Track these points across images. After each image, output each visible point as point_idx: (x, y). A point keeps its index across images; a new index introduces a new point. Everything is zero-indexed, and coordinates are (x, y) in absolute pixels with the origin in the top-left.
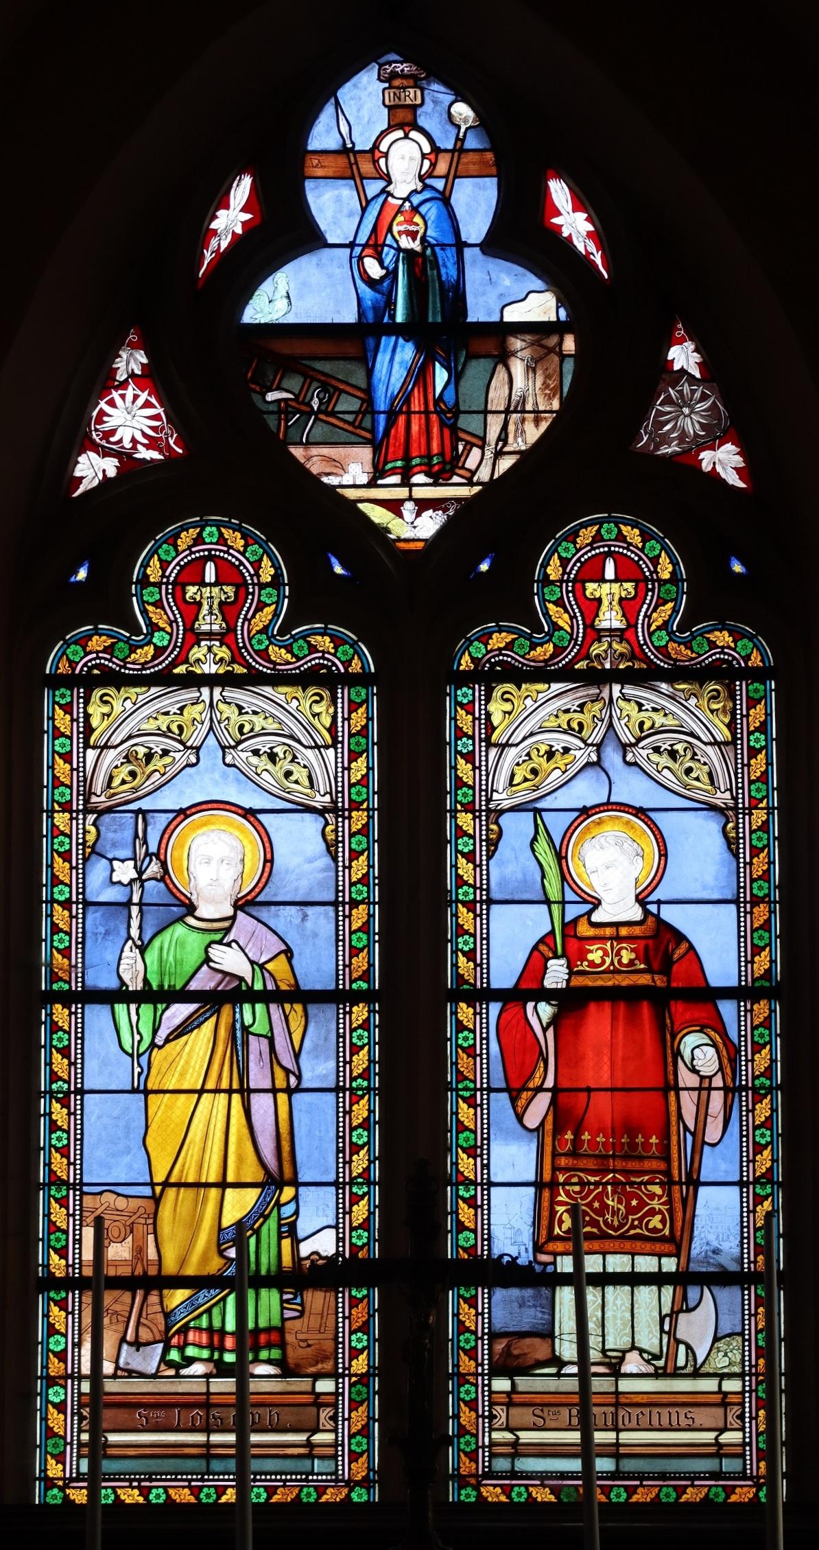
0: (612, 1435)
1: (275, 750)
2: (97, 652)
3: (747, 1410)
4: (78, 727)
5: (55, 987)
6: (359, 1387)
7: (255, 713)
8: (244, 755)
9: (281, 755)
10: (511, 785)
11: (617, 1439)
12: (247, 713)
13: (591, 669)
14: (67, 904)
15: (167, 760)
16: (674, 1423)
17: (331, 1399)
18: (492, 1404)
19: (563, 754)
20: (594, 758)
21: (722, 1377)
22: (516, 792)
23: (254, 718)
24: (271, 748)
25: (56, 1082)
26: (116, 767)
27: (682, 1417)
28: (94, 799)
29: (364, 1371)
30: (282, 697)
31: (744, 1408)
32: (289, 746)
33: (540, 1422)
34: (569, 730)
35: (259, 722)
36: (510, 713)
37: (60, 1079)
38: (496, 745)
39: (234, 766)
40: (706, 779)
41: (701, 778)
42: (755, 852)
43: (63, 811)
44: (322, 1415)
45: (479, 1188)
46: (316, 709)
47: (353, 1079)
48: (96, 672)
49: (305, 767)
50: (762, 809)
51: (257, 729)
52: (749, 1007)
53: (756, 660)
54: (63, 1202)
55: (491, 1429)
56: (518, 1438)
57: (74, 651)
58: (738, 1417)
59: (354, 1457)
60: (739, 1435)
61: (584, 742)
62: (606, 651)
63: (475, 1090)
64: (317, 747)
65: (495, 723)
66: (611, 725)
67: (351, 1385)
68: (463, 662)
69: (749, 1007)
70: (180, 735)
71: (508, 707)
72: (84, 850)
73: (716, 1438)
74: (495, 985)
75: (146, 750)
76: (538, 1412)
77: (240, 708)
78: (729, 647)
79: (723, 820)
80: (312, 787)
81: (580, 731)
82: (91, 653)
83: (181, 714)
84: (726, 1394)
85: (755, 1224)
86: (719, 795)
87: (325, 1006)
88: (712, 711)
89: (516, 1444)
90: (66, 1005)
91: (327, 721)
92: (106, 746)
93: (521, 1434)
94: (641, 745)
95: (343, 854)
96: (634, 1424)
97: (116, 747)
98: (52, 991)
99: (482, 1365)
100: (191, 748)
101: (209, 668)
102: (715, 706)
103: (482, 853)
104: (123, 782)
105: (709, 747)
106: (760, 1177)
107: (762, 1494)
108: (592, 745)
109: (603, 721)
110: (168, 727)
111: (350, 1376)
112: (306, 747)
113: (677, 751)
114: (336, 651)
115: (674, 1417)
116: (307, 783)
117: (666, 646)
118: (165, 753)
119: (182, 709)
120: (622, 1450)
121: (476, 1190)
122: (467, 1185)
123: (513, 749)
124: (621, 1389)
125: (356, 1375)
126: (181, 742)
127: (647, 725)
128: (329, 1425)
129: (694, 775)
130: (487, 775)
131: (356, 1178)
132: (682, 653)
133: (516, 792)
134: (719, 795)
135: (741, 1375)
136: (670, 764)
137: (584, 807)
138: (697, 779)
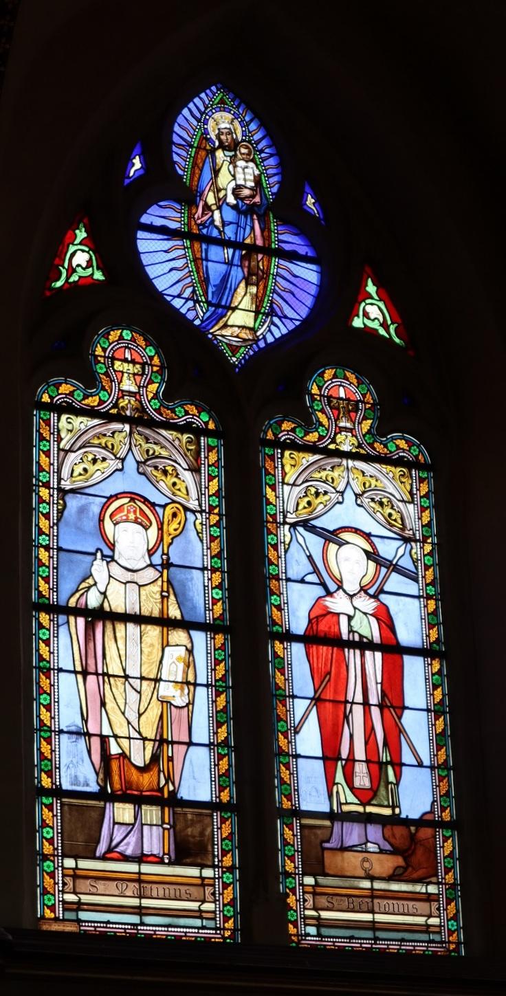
2: (288, 431)
3: (217, 889)
4: (54, 438)
7: (371, 476)
8: (149, 469)
9: (386, 504)
10: (72, 476)
11: (374, 919)
12: (151, 443)
14: (47, 548)
15: (327, 497)
16: (396, 910)
17: (211, 882)
18: (64, 876)
19: (102, 461)
20: (120, 466)
22: (74, 482)
23: (154, 446)
24: (164, 467)
26: (76, 464)
28: (63, 482)
29: (230, 864)
30: (385, 470)
31: (215, 888)
32: (174, 467)
33: (94, 890)
34: (105, 448)
37: (45, 660)
38: (63, 450)
39: (362, 506)
40: (184, 491)
41: (182, 489)
44: (207, 892)
45: (53, 734)
47: (216, 681)
48: (288, 441)
49: (398, 512)
50: (429, 543)
55: (305, 908)
56: (80, 899)
58: (66, 884)
61: (115, 456)
62: (127, 405)
66: (348, 482)
67: (446, 890)
68: (268, 434)
69: (212, 636)
71: (293, 463)
72: (284, 546)
73: (426, 921)
75: (93, 456)
76: (329, 899)
77: (363, 473)
80: (188, 494)
81: (333, 482)
87: (155, 627)
88: (402, 482)
90: (282, 642)
92: (70, 450)
93: (82, 897)
94: (366, 495)
96: (382, 910)
97: (75, 452)
99: (57, 849)
100: (119, 458)
101: (345, 448)
102: (190, 448)
104: (305, 508)
105: (187, 472)
108: (119, 458)
109: (125, 445)
110: (106, 444)
111: (222, 867)
115: (167, 891)
116: (185, 492)
118: (326, 493)
120: (144, 911)
124: (142, 871)
125: (448, 884)
126: (113, 454)
127: (151, 452)
128: (211, 898)
130: (283, 503)
133: (74, 482)
134: (407, 532)
136: (380, 510)
137: (154, 503)
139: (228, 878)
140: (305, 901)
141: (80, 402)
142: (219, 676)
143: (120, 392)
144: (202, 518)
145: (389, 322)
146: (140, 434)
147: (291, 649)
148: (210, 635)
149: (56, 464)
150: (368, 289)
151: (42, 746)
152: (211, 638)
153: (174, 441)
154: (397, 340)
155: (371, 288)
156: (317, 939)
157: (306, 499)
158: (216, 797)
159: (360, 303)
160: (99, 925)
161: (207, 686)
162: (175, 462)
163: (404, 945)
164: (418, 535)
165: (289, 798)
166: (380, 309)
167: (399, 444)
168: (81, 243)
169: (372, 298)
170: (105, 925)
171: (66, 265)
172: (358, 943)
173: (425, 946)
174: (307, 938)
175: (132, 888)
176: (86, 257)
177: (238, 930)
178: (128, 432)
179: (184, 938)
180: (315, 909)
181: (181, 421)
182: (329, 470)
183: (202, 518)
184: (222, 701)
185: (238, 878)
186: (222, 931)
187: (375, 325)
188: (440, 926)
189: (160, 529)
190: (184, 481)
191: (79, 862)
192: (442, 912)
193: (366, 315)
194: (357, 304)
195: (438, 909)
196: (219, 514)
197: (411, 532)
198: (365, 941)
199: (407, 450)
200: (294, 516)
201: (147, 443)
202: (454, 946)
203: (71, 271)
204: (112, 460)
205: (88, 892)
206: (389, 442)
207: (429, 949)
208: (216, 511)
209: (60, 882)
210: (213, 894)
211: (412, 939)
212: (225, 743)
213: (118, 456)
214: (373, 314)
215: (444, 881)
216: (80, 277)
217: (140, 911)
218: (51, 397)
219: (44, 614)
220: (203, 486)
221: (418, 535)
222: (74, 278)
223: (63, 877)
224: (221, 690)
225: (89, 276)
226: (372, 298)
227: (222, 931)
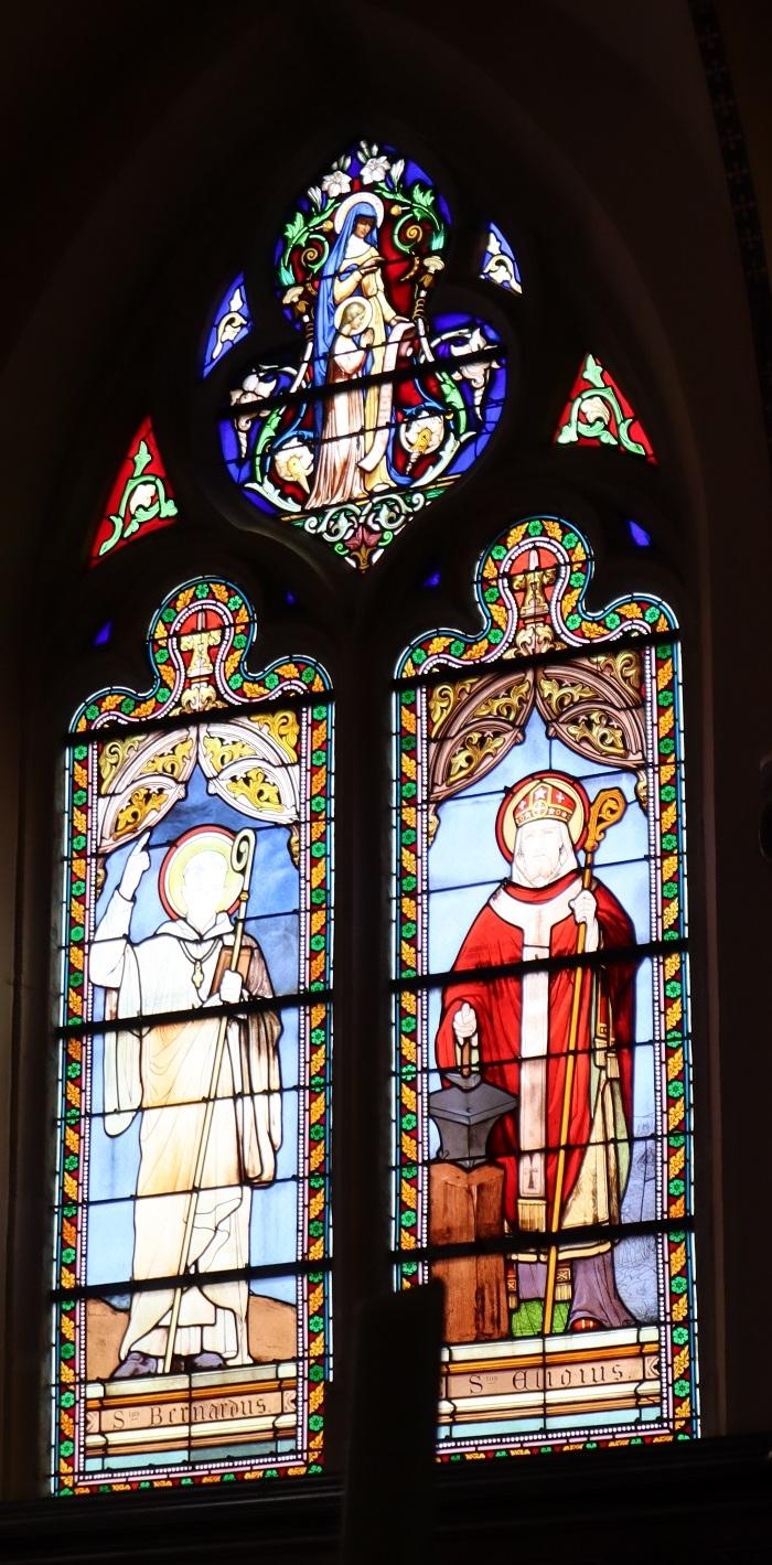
0: (540, 1396)
1: (249, 775)
2: (438, 654)
5: (404, 975)
6: (316, 1367)
7: (234, 743)
9: (597, 721)
10: (116, 831)
11: (190, 1433)
12: (567, 686)
13: (182, 714)
16: (598, 1378)
18: (87, 1410)
19: (158, 795)
21: (277, 1362)
23: (233, 748)
25: (406, 1066)
27: (254, 1405)
33: (119, 1425)
34: (156, 774)
35: (237, 750)
36: (116, 764)
42: (664, 805)
43: (80, 858)
46: (283, 730)
48: (435, 670)
51: (236, 757)
52: (661, 960)
53: (318, 687)
54: (413, 1182)
55: (87, 1434)
56: (455, 1407)
57: (92, 712)
59: (678, 1401)
60: (656, 1385)
63: (80, 1116)
64: (284, 765)
65: (104, 776)
66: (197, 762)
67: (310, 1367)
70: (172, 773)
73: (635, 1391)
74: (433, 971)
75: (480, 735)
77: (222, 740)
78: (296, 678)
79: (635, 781)
82: (432, 655)
83: (174, 754)
84: (282, 1380)
85: (668, 1176)
86: (631, 757)
89: (106, 1446)
90: (414, 992)
91: (294, 741)
92: (113, 794)
95: (304, 859)
98: (401, 979)
103: (91, 893)
106: (673, 1130)
107: (67, 1490)
111: (671, 1323)
112: (275, 766)
113: (593, 721)
114: (644, 615)
117: (580, 627)
119: (173, 749)
121: (77, 1209)
122: (411, 1166)
123: (118, 797)
125: (314, 1358)
129: (609, 741)
131: (314, 1172)
132: (253, 690)
135: (295, 1360)
138: (612, 745)
139: (681, 1336)
140: (295, 1401)
141: (459, 658)
142: (672, 1023)
143: (521, 622)
144: (648, 778)
145: (619, 418)
146: (548, 679)
147: (92, 1046)
148: (304, 1010)
149: (425, 765)
150: (586, 375)
151: (403, 1191)
152: (305, 1015)
153: (260, 729)
154: (631, 447)
155: (593, 371)
156: (186, 1468)
157: (133, 809)
158: (663, 1212)
159: (573, 401)
160: (619, 1429)
161: (297, 1088)
162: (605, 702)
163: (595, 1435)
164: (650, 756)
165: (72, 1267)
166: (604, 399)
167: (287, 675)
168: (143, 474)
169: (595, 388)
170: (499, 1440)
171: (122, 513)
172: (163, 1473)
173: (585, 1436)
174: (639, 1428)
175: (177, 1411)
176: (150, 489)
177: (697, 1417)
178: (532, 681)
179: (566, 1448)
180: (102, 1433)
181: (615, 636)
182: (504, 696)
183: (648, 778)
184: (676, 1062)
185: (696, 1331)
186: (671, 1423)
187: (595, 431)
188: (660, 1394)
189: (587, 814)
190: (274, 785)
191: (108, 1388)
192: (664, 1370)
193: (582, 417)
194: (569, 404)
195: (658, 1367)
196: (677, 763)
197: (639, 756)
198: (257, 1461)
199: (296, 678)
200: (444, 787)
201: (561, 688)
202: (683, 1423)
203: (129, 517)
204: (509, 731)
205: (469, 1394)
206: (242, 676)
207: (592, 1439)
208: (671, 759)
209: (300, 1404)
210: (295, 1401)
211: (248, 1454)
212: (681, 1129)
213: (180, 780)
214: (594, 413)
215: (306, 1355)
216: (140, 524)
217: (190, 1443)
218: (416, 666)
219: (407, 994)
220: (649, 723)
221: (650, 756)
222: (134, 527)
223: (85, 1412)
224: (318, 1090)
225: (154, 517)
226: (595, 388)
227: (671, 1423)
